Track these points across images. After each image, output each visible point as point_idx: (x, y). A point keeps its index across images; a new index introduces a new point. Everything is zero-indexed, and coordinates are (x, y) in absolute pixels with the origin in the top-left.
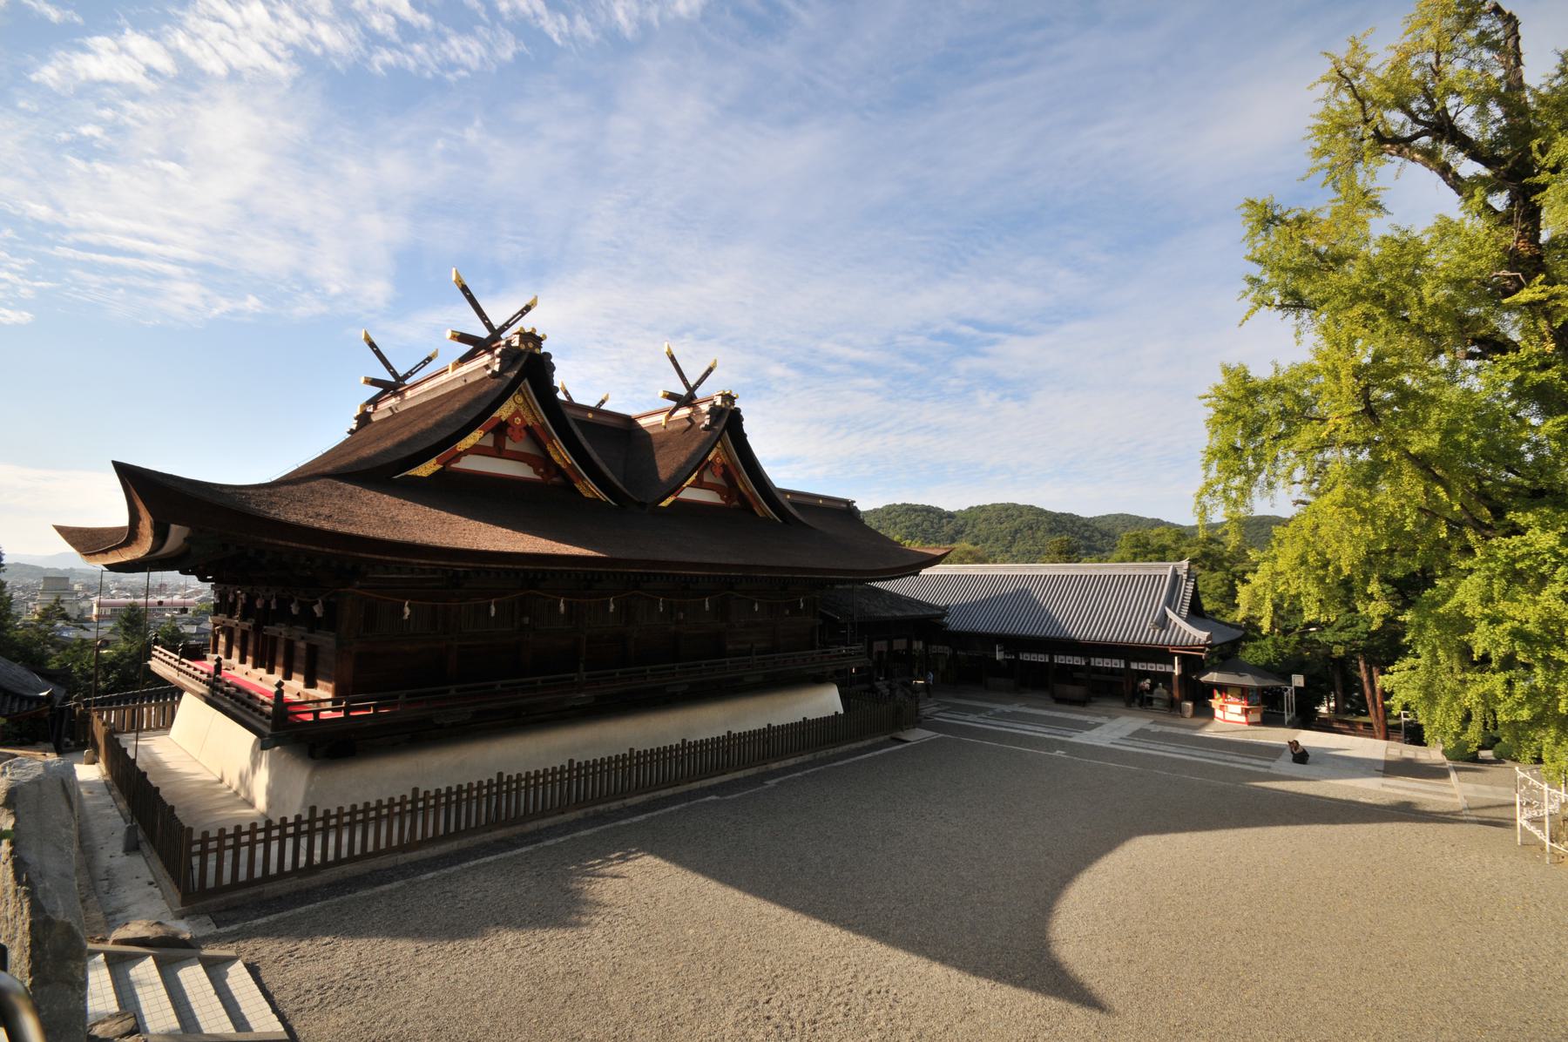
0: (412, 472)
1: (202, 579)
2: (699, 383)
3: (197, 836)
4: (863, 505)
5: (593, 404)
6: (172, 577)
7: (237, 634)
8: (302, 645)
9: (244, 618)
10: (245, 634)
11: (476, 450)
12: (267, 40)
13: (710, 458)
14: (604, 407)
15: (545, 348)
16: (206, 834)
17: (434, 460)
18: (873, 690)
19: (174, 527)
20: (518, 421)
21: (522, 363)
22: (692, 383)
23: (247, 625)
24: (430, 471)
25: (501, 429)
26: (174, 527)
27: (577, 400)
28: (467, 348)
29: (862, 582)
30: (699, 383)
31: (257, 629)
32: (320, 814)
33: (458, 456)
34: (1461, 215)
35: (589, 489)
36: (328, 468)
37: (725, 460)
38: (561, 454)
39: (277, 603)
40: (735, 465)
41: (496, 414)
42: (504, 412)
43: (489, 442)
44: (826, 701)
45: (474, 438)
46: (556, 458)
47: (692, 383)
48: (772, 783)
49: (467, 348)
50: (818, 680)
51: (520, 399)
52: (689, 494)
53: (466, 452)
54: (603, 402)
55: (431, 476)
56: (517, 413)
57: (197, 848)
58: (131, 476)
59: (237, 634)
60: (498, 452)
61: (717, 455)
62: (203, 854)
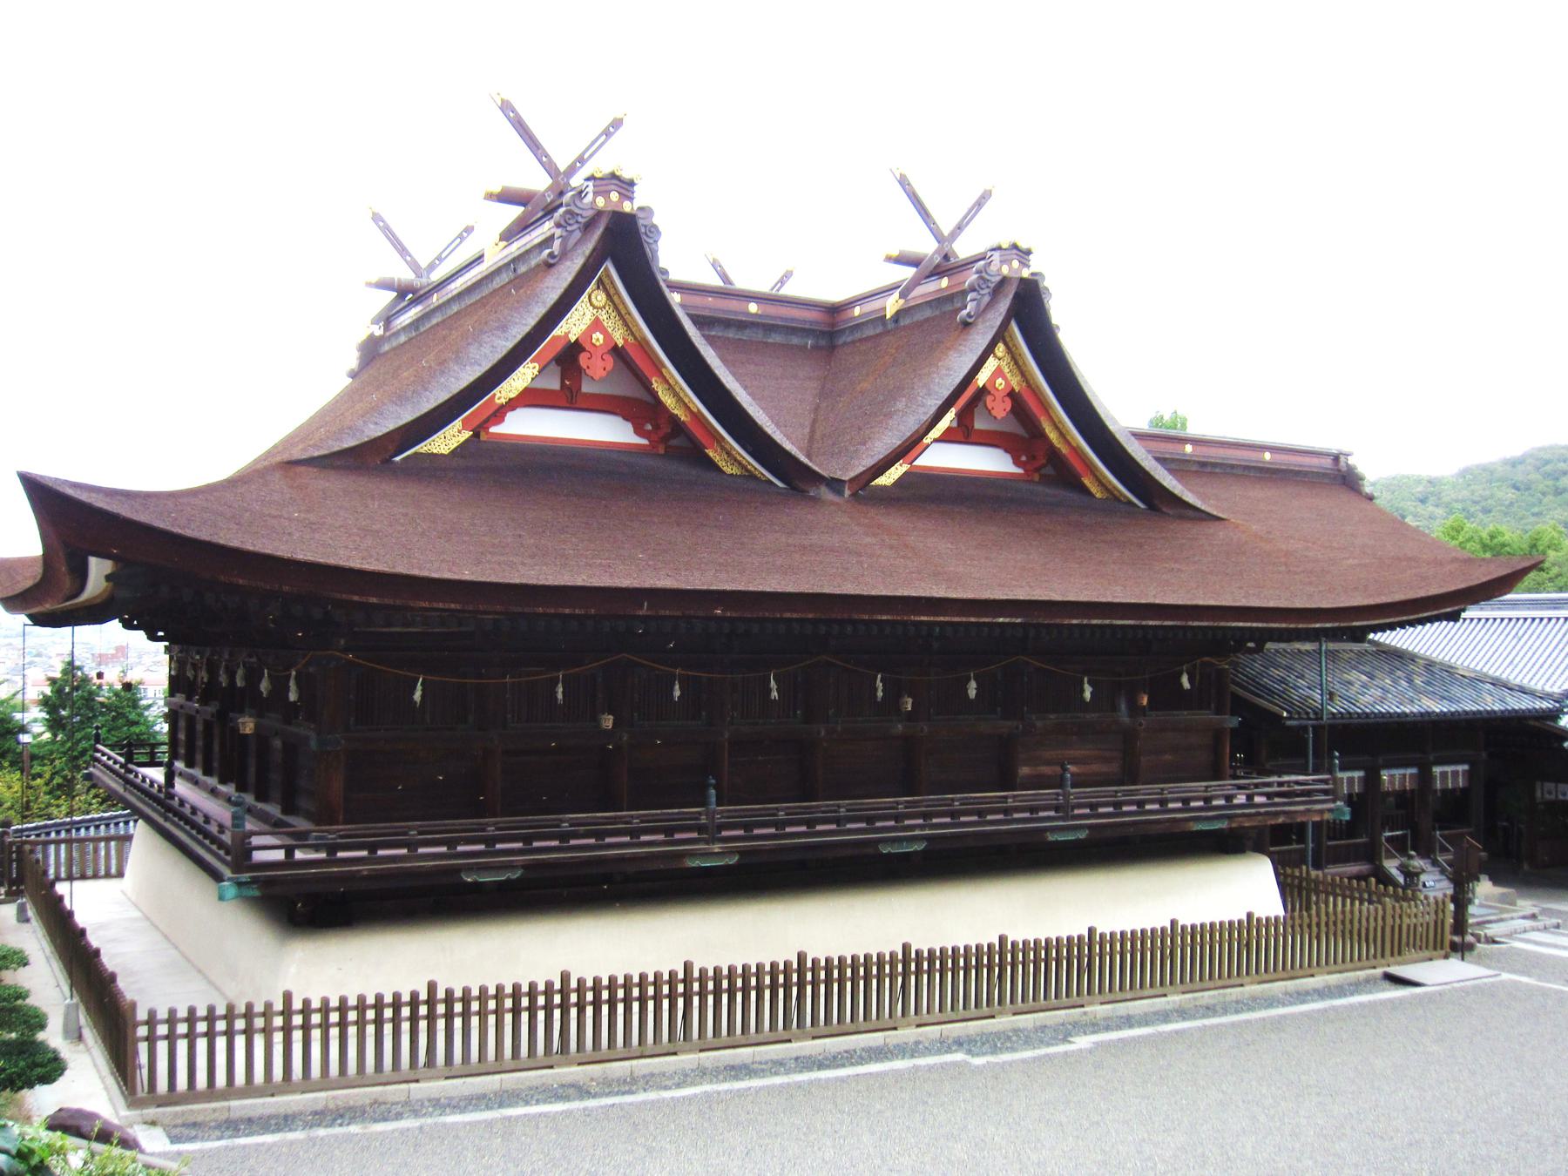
0: (423, 448)
1: (153, 637)
2: (960, 227)
3: (142, 1015)
4: (1372, 469)
5: (763, 286)
6: (112, 632)
7: (200, 727)
8: (277, 743)
9: (204, 701)
10: (208, 725)
11: (531, 398)
12: (8, 641)
13: (982, 378)
14: (788, 291)
15: (641, 198)
16: (152, 1013)
17: (458, 423)
18: (1385, 879)
19: (93, 562)
20: (598, 338)
21: (598, 233)
22: (946, 230)
23: (211, 709)
24: (454, 444)
25: (570, 358)
26: (93, 562)
27: (741, 283)
28: (516, 211)
29: (1359, 635)
30: (960, 227)
31: (222, 715)
32: (297, 1005)
33: (499, 414)
34: (124, 1112)
35: (730, 455)
36: (297, 453)
37: (1015, 382)
38: (676, 395)
39: (246, 678)
40: (642, 345)
41: (558, 331)
42: (573, 326)
43: (554, 384)
44: (1245, 889)
45: (523, 377)
46: (668, 400)
47: (946, 230)
48: (1083, 1042)
49: (516, 211)
50: (1224, 843)
51: (600, 298)
52: (942, 457)
53: (512, 404)
54: (782, 282)
55: (454, 452)
56: (597, 325)
57: (142, 1031)
58: (42, 494)
59: (200, 727)
60: (569, 398)
61: (998, 372)
62: (151, 1039)
